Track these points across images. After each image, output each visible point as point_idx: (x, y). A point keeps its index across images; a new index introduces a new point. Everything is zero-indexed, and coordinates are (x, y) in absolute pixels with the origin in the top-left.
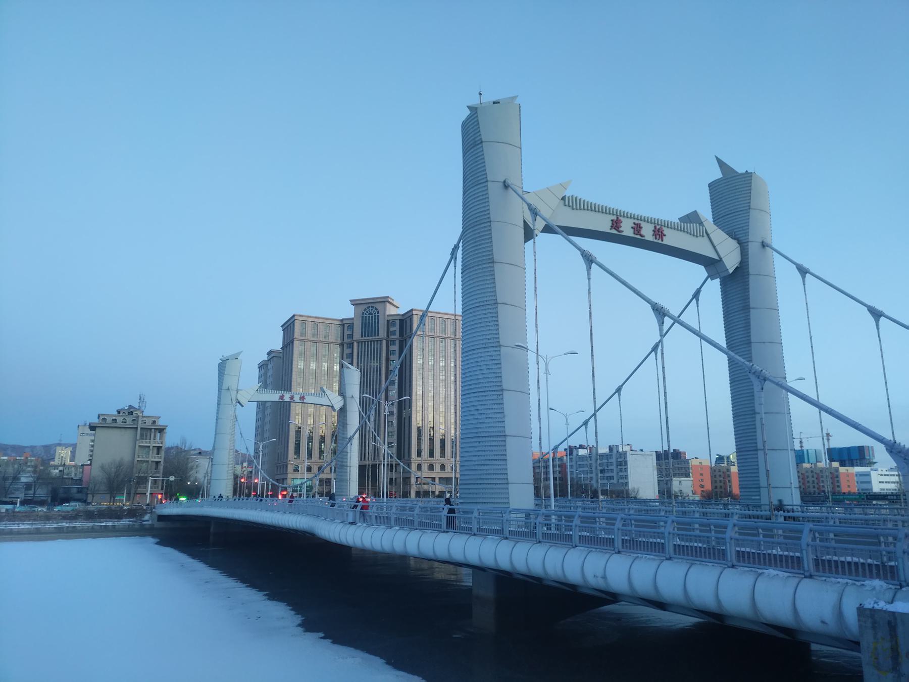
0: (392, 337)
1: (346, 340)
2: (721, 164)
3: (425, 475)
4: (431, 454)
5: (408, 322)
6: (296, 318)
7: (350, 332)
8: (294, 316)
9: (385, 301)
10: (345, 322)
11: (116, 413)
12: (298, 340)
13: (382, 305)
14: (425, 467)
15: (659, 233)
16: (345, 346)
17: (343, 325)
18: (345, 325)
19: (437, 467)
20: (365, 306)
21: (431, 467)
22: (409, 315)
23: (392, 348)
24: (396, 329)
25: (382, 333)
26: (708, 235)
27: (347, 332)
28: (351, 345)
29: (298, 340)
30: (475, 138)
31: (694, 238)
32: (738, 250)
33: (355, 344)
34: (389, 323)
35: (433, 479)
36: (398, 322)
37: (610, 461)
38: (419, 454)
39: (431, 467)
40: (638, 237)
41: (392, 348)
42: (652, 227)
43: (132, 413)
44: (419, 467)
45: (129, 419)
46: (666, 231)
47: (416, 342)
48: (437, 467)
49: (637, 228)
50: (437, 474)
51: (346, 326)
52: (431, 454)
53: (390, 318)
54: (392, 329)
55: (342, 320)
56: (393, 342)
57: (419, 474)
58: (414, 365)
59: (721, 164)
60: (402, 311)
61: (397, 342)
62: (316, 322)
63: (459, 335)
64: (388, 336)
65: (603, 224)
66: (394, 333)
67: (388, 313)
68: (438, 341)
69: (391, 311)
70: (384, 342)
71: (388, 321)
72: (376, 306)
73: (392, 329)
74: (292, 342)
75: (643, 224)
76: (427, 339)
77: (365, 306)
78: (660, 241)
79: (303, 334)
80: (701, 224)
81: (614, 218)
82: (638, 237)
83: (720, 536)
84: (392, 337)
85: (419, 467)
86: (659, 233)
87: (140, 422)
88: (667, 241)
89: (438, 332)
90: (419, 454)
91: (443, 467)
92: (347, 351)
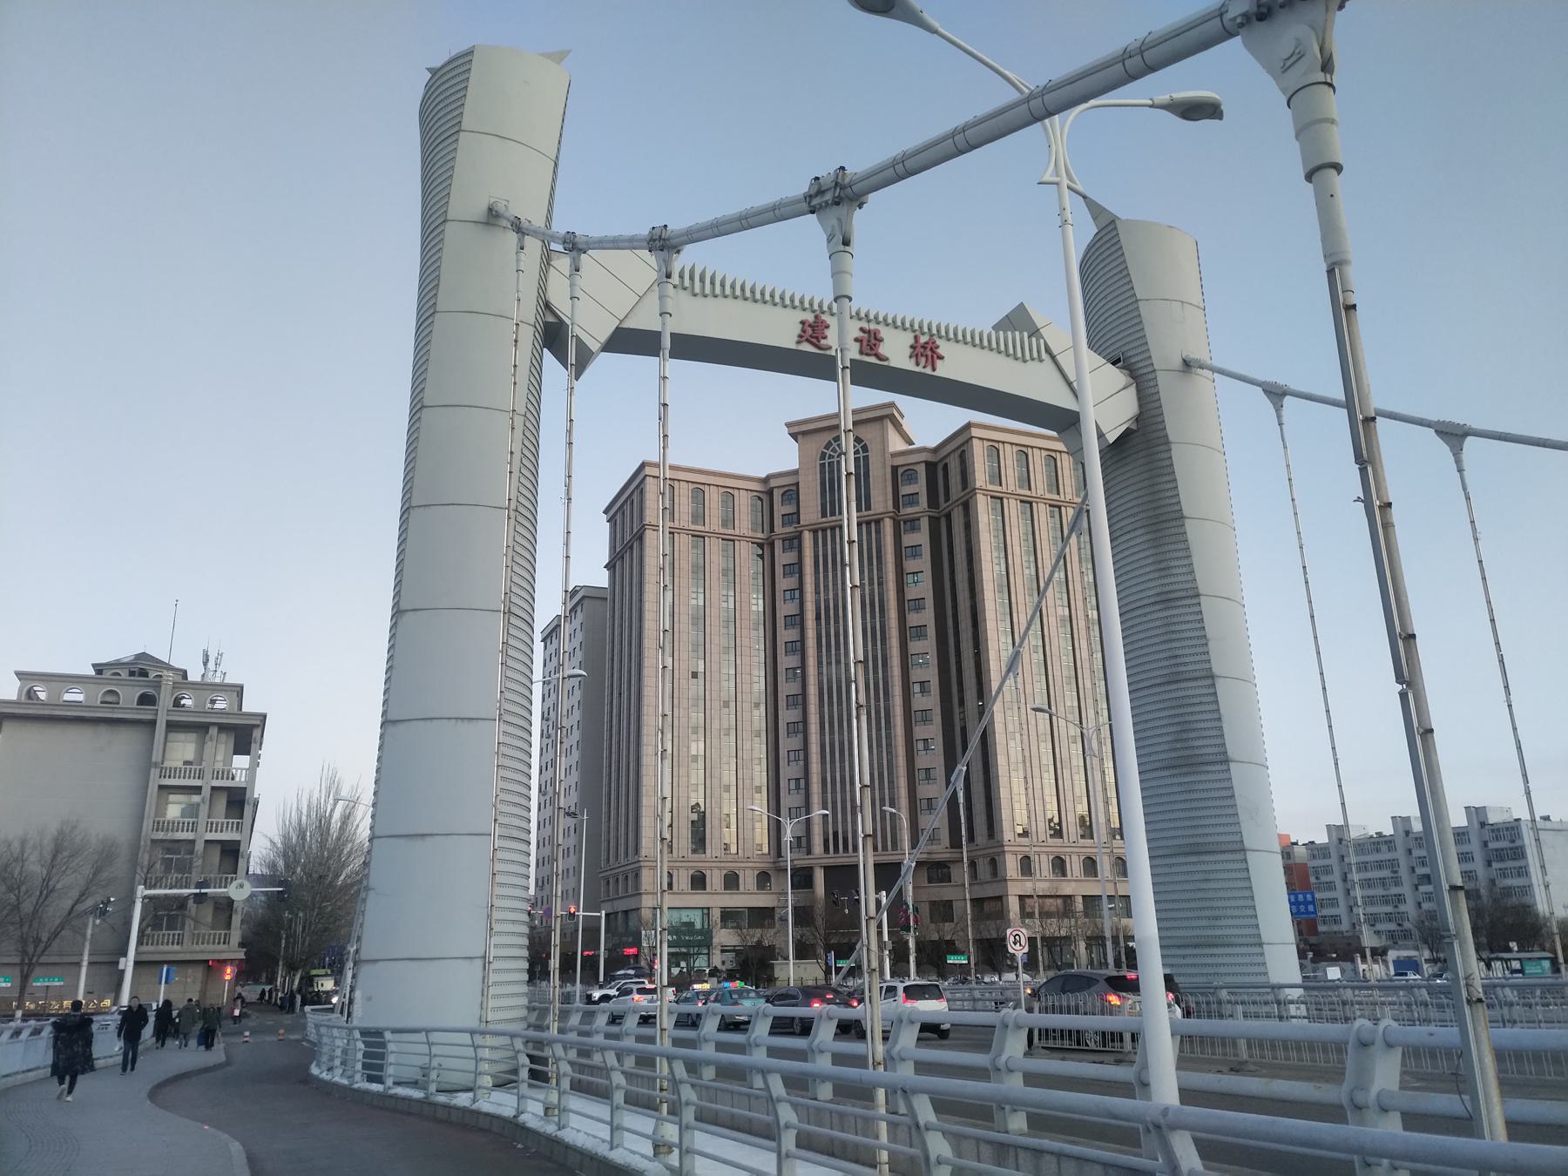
0: (908, 511)
1: (778, 529)
3: (1042, 887)
5: (954, 465)
6: (648, 470)
7: (789, 509)
8: (643, 466)
10: (773, 483)
13: (876, 426)
15: (926, 350)
16: (778, 545)
17: (770, 493)
18: (774, 494)
24: (920, 487)
26: (1053, 357)
27: (780, 509)
28: (794, 542)
30: (444, 105)
31: (1019, 365)
32: (1132, 391)
33: (807, 537)
34: (899, 475)
35: (1068, 898)
36: (921, 470)
37: (1402, 908)
40: (873, 360)
41: (909, 539)
42: (908, 338)
43: (144, 673)
44: (1026, 865)
45: (129, 695)
46: (944, 348)
49: (870, 341)
51: (777, 495)
53: (899, 461)
55: (766, 480)
56: (913, 524)
57: (1027, 887)
61: (924, 523)
62: (700, 485)
63: (984, 511)
65: (782, 331)
66: (912, 499)
70: (888, 526)
71: (895, 469)
73: (905, 490)
74: (640, 537)
75: (885, 332)
78: (928, 371)
80: (1035, 332)
81: (810, 317)
82: (873, 360)
83: (1445, 1103)
84: (908, 511)
85: (1026, 865)
86: (926, 350)
87: (165, 701)
88: (943, 370)
92: (783, 558)
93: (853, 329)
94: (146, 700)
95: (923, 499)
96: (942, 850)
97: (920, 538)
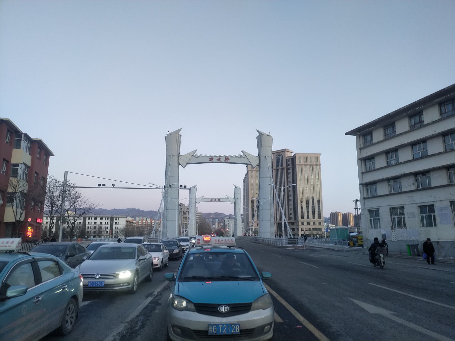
0: (289, 167)
2: (258, 131)
4: (308, 217)
9: (284, 151)
11: (97, 186)
12: (298, 165)
14: (306, 223)
19: (311, 223)
20: (277, 154)
21: (308, 223)
22: (295, 156)
23: (289, 171)
24: (290, 163)
25: (284, 165)
29: (298, 165)
35: (310, 228)
36: (291, 160)
38: (302, 217)
39: (308, 223)
41: (289, 171)
46: (230, 158)
47: (298, 169)
48: (311, 223)
50: (311, 226)
52: (308, 217)
54: (288, 163)
56: (289, 169)
58: (297, 179)
59: (258, 131)
60: (293, 154)
61: (291, 169)
64: (287, 166)
66: (289, 165)
67: (286, 156)
68: (309, 166)
69: (288, 155)
70: (285, 169)
71: (287, 160)
72: (282, 153)
73: (288, 163)
76: (303, 167)
77: (277, 154)
79: (300, 162)
84: (289, 167)
88: (229, 161)
89: (309, 163)
90: (302, 217)
91: (314, 223)
93: (217, 158)
94: (181, 209)
95: (291, 164)
96: (292, 221)
97: (290, 171)
